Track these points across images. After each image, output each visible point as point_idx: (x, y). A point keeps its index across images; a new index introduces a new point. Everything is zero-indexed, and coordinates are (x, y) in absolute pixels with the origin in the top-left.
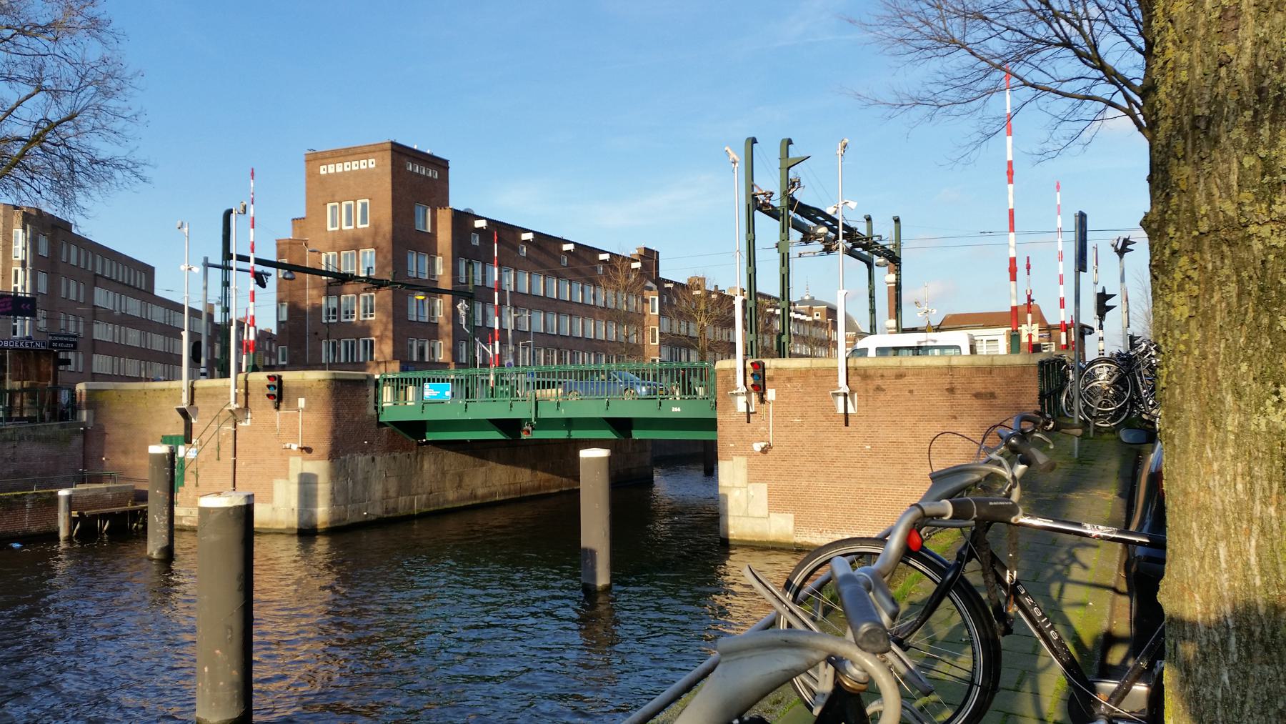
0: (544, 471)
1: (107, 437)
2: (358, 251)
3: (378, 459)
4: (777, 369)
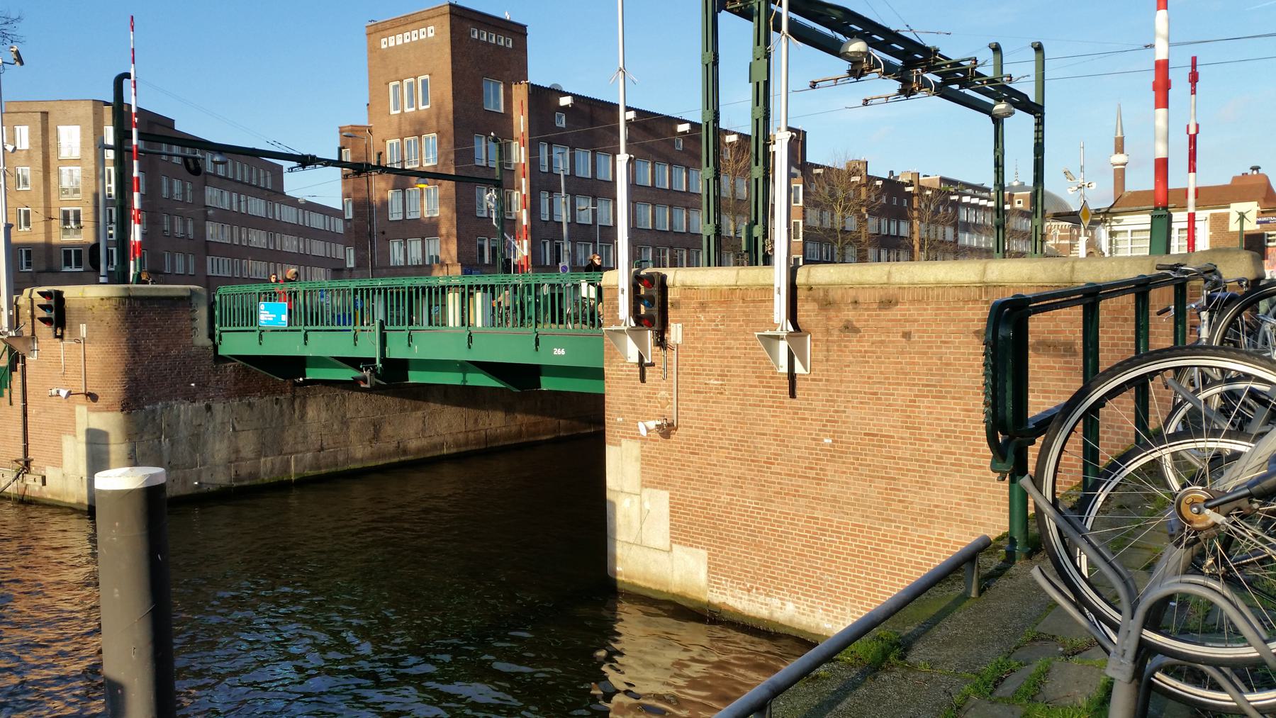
0: (527, 412)
2: (420, 136)
3: (218, 407)
4: (686, 287)
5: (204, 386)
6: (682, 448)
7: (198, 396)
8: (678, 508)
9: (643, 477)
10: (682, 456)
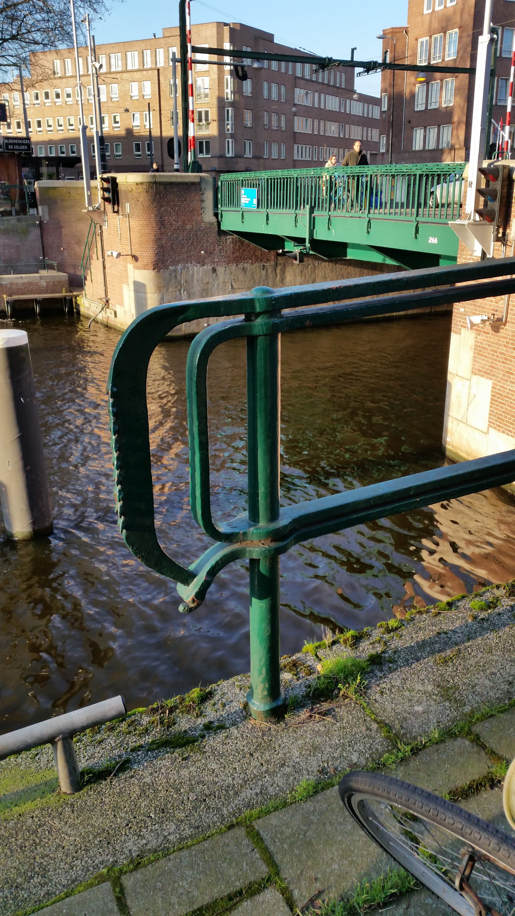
1: (63, 229)
2: (445, 33)
3: (220, 270)
5: (211, 253)
6: (508, 343)
7: (206, 261)
8: (498, 397)
9: (474, 365)
10: (507, 351)
